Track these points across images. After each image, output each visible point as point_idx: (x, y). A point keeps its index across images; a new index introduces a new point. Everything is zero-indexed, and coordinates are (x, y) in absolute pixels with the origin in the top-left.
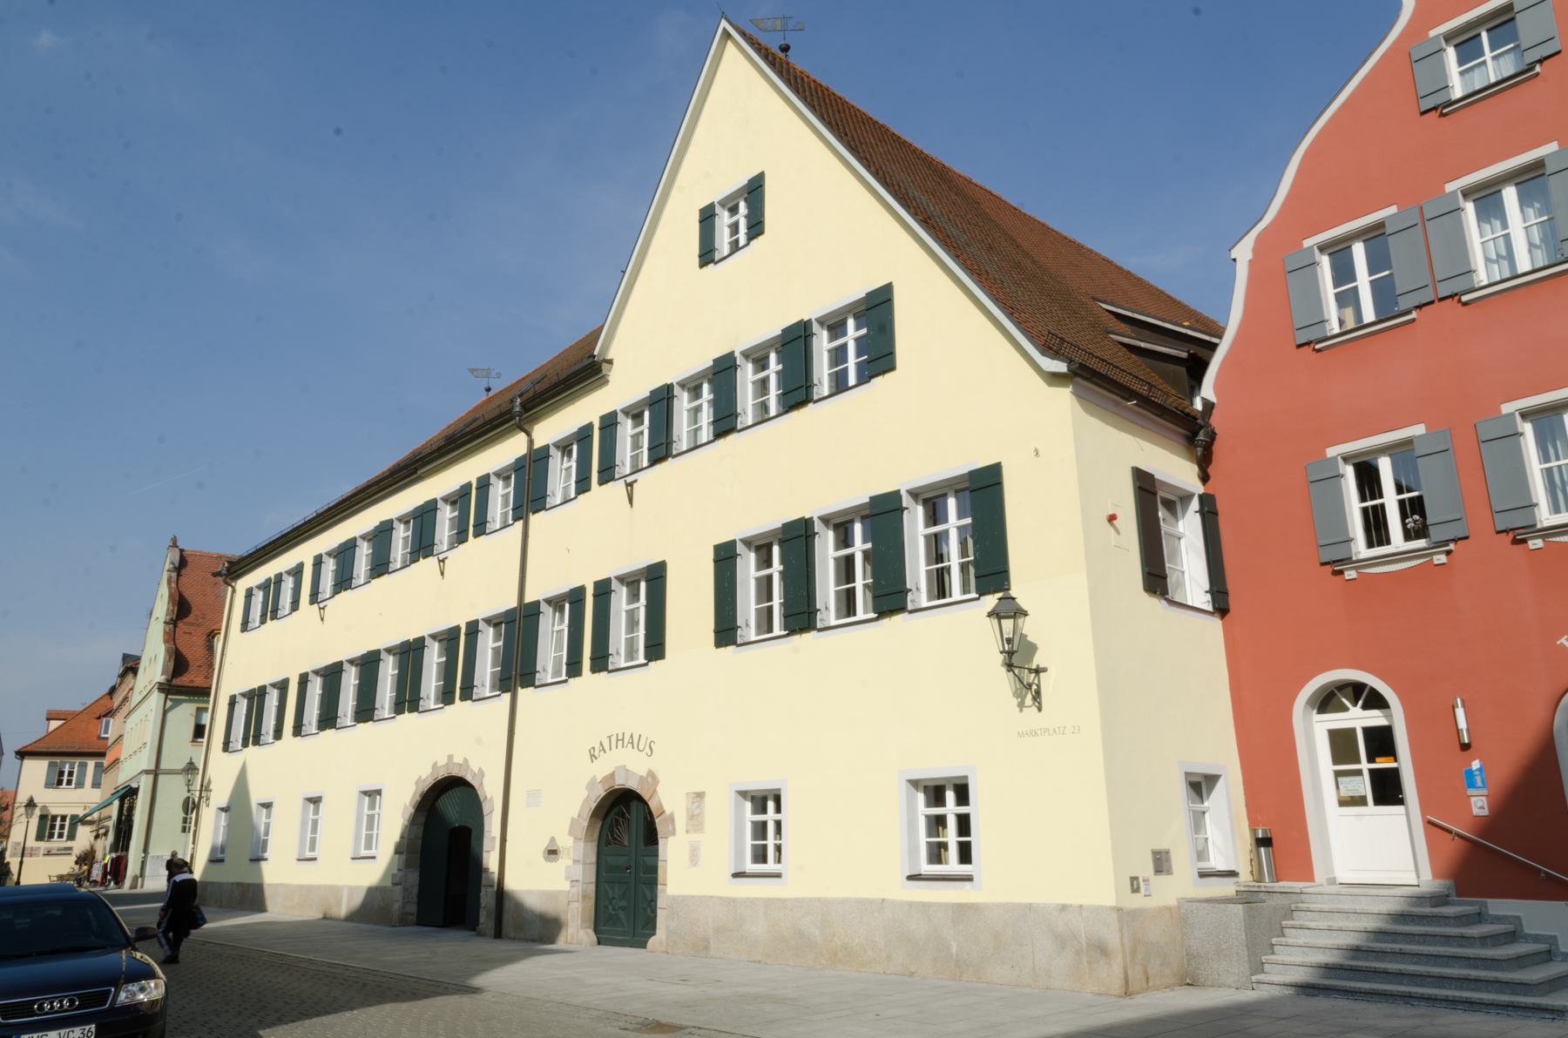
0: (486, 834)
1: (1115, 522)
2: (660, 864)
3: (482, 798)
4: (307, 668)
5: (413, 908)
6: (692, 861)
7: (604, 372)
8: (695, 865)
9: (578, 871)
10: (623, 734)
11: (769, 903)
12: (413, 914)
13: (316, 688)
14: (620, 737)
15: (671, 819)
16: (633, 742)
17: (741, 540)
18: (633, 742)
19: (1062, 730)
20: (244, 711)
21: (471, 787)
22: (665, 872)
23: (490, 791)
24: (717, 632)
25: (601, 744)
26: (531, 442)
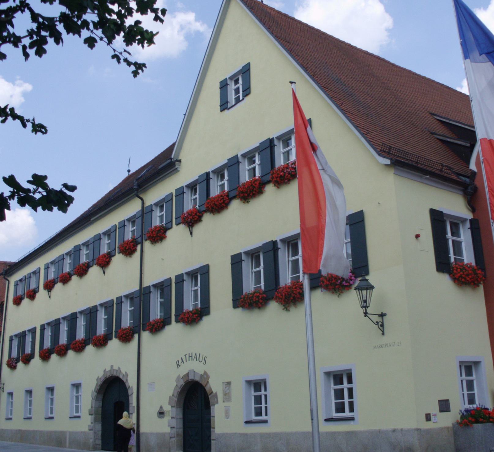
0: (130, 405)
1: (419, 238)
2: (212, 418)
3: (127, 387)
4: (44, 322)
5: (99, 442)
6: (226, 416)
7: (177, 167)
8: (228, 418)
9: (174, 423)
10: (192, 353)
11: (262, 435)
12: (100, 445)
13: (48, 333)
14: (190, 355)
15: (216, 395)
16: (196, 357)
17: (244, 252)
18: (196, 357)
19: (393, 344)
20: (31, 340)
21: (123, 381)
22: (214, 422)
23: (131, 382)
24: (233, 300)
25: (182, 359)
26: (143, 203)
